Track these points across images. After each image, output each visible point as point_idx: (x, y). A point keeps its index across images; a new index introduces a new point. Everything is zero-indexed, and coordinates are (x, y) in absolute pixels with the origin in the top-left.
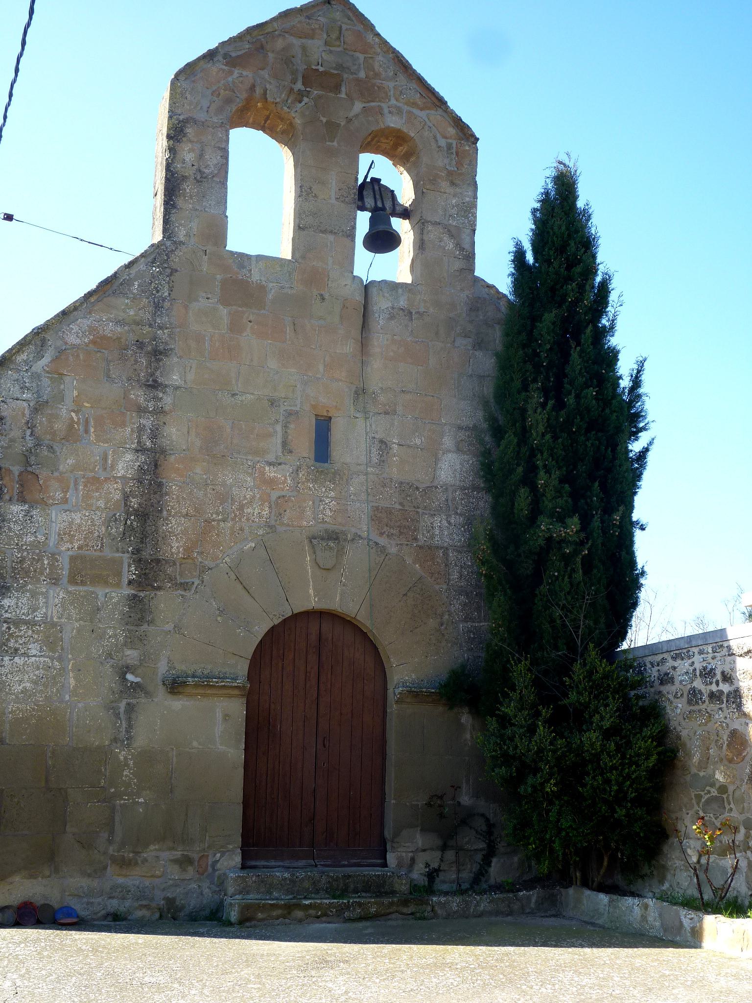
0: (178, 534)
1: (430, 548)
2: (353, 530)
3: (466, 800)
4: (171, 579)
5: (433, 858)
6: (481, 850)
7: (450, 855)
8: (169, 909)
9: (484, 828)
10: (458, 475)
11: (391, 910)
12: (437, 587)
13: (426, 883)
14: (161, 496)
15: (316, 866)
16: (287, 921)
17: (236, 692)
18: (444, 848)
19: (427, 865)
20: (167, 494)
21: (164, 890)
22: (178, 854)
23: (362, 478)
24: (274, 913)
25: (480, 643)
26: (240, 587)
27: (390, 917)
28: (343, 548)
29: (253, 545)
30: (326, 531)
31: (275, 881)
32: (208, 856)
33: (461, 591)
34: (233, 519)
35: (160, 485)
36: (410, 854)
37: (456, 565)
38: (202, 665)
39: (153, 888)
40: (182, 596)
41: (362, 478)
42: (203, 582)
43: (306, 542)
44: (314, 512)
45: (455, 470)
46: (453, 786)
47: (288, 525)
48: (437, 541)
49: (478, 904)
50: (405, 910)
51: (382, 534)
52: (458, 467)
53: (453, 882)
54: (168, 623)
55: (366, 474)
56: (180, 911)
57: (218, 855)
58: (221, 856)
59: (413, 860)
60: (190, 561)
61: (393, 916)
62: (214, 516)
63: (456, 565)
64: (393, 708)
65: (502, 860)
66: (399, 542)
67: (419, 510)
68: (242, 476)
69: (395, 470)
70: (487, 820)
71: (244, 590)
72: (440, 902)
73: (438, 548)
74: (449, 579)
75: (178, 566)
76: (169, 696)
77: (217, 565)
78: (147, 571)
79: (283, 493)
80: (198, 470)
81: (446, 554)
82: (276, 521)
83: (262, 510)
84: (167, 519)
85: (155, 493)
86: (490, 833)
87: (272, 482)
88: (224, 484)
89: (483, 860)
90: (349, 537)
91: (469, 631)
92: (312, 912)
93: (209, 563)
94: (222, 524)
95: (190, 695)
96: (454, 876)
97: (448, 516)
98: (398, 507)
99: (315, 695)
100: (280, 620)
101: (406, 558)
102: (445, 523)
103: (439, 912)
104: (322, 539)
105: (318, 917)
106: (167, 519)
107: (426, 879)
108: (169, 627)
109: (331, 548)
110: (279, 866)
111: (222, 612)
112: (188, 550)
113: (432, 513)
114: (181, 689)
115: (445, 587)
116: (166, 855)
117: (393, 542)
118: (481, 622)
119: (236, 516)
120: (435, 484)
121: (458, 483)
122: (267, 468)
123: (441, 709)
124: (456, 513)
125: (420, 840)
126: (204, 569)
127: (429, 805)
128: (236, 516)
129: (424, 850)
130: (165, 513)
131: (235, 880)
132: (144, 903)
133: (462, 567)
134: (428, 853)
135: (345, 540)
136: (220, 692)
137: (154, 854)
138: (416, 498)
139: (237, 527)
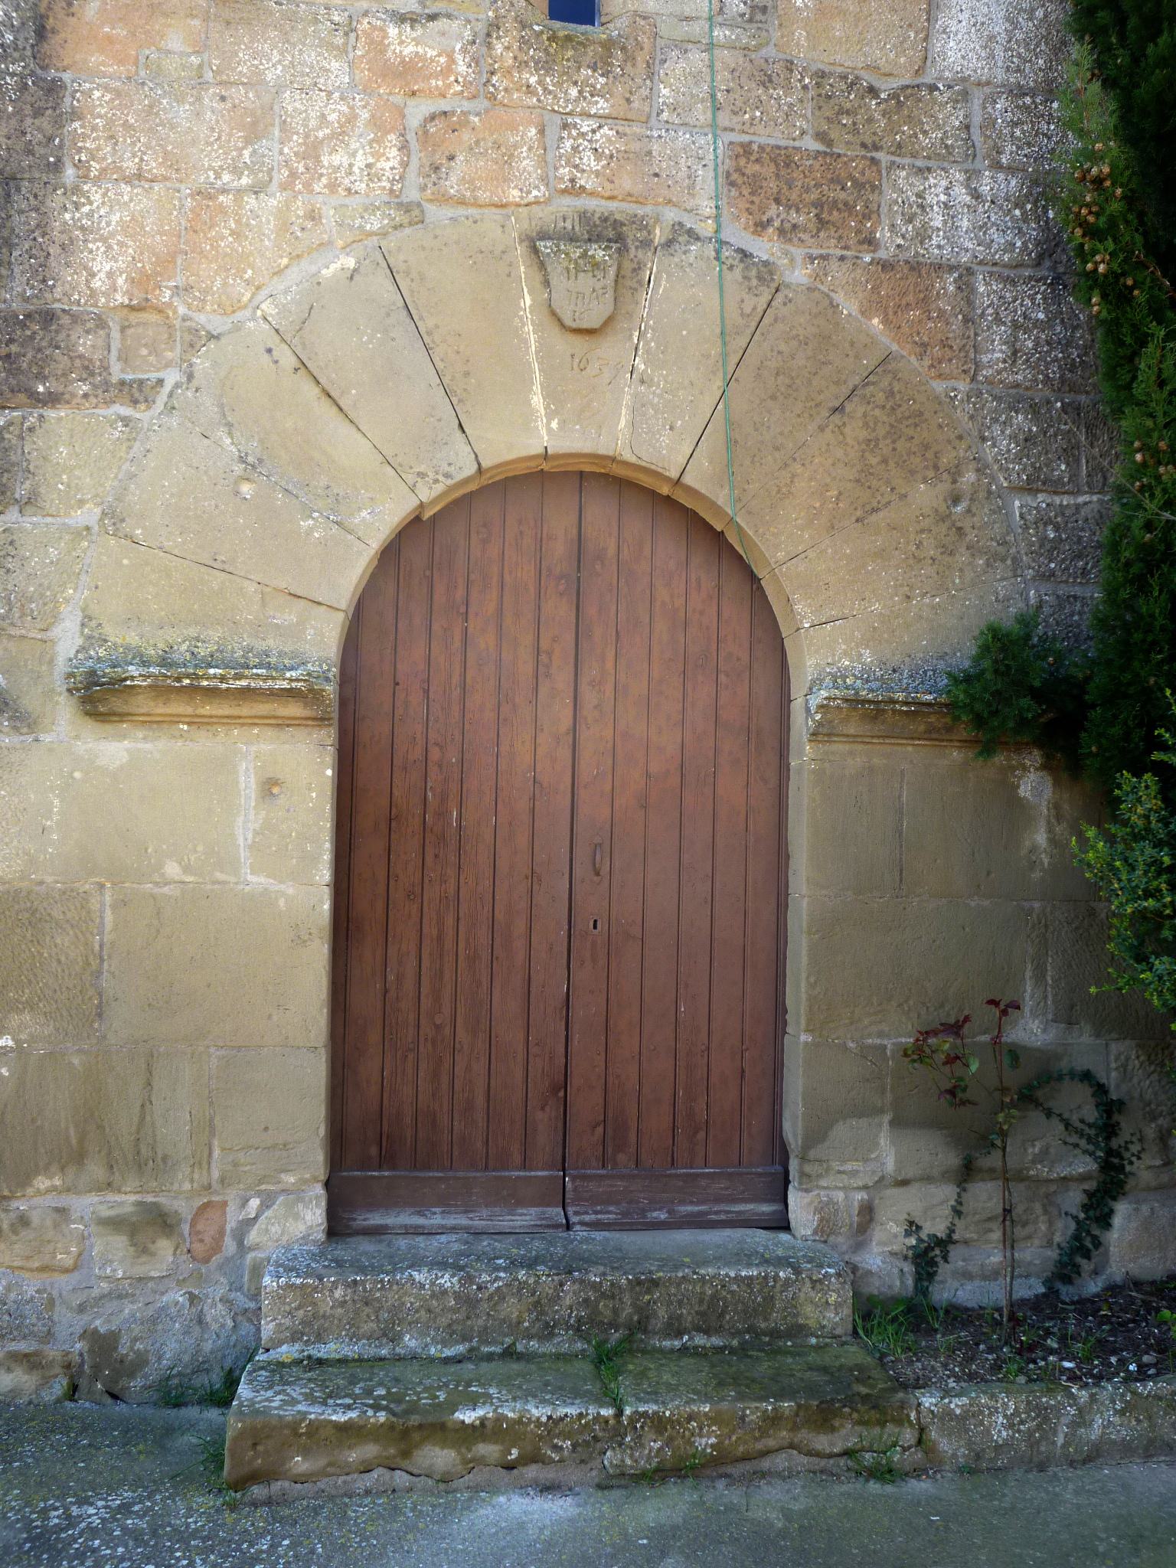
0: (112, 235)
1: (915, 267)
2: (671, 215)
3: (1031, 1030)
4: (88, 371)
5: (932, 1207)
6: (1083, 1178)
7: (985, 1196)
8: (97, 1368)
9: (1091, 1113)
10: (999, 52)
11: (771, 1443)
12: (939, 387)
13: (910, 1282)
14: (59, 122)
15: (568, 1227)
16: (401, 1478)
17: (294, 709)
18: (967, 1173)
19: (913, 1227)
20: (75, 115)
21: (81, 1309)
22: (125, 1201)
23: (697, 58)
24: (353, 1456)
25: (1080, 556)
26: (311, 391)
27: (765, 1464)
28: (637, 269)
29: (351, 263)
30: (584, 216)
31: (408, 1301)
32: (225, 1203)
33: (1016, 399)
34: (283, 187)
35: (54, 89)
36: (860, 1196)
37: (998, 320)
38: (192, 632)
39: (51, 1303)
40: (126, 421)
41: (697, 58)
42: (190, 377)
43: (520, 250)
44: (543, 161)
45: (992, 38)
46: (992, 1002)
47: (462, 202)
48: (937, 247)
49: (1082, 1420)
50: (822, 1442)
51: (761, 226)
52: (1000, 28)
53: (995, 1275)
54: (81, 503)
55: (710, 47)
56: (132, 1375)
57: (255, 1203)
58: (265, 1206)
59: (868, 1212)
60: (151, 317)
61: (780, 1461)
62: (226, 177)
63: (998, 320)
64: (804, 754)
65: (1145, 1209)
66: (816, 252)
67: (878, 155)
68: (310, 56)
69: (800, 34)
70: (1101, 1089)
71: (326, 403)
72: (949, 1414)
73: (940, 268)
74: (978, 365)
75: (116, 334)
76: (90, 723)
77: (237, 327)
78: (14, 348)
79: (444, 105)
80: (175, 42)
81: (965, 286)
82: (423, 188)
83: (378, 156)
84: (76, 190)
85: (38, 113)
86: (1109, 1129)
87: (407, 72)
88: (255, 81)
89: (1085, 1208)
90: (658, 235)
91: (1043, 521)
92: (488, 1450)
93: (208, 319)
94: (251, 201)
95: (151, 722)
96: (996, 1259)
97: (972, 175)
98: (812, 144)
99: (566, 722)
100: (439, 488)
101: (839, 297)
102: (961, 194)
103: (944, 1445)
104: (572, 239)
105: (510, 1467)
106: (76, 190)
107: (909, 1268)
108: (87, 515)
109: (596, 265)
110: (454, 1229)
111: (252, 467)
112: (143, 281)
113: (919, 163)
114: (117, 704)
115: (963, 386)
116: (87, 1204)
117: (799, 252)
118: (1079, 492)
119: (293, 175)
120: (928, 80)
121: (1000, 76)
122: (393, 31)
123: (956, 755)
124: (997, 166)
125: (888, 1153)
126: (197, 339)
127: (918, 1053)
128: (293, 175)
129: (904, 1183)
130: (70, 172)
131: (279, 1298)
132: (22, 1346)
133: (1016, 326)
134: (913, 1189)
135: (646, 244)
136: (245, 710)
137: (52, 1201)
138: (870, 120)
139: (299, 207)
